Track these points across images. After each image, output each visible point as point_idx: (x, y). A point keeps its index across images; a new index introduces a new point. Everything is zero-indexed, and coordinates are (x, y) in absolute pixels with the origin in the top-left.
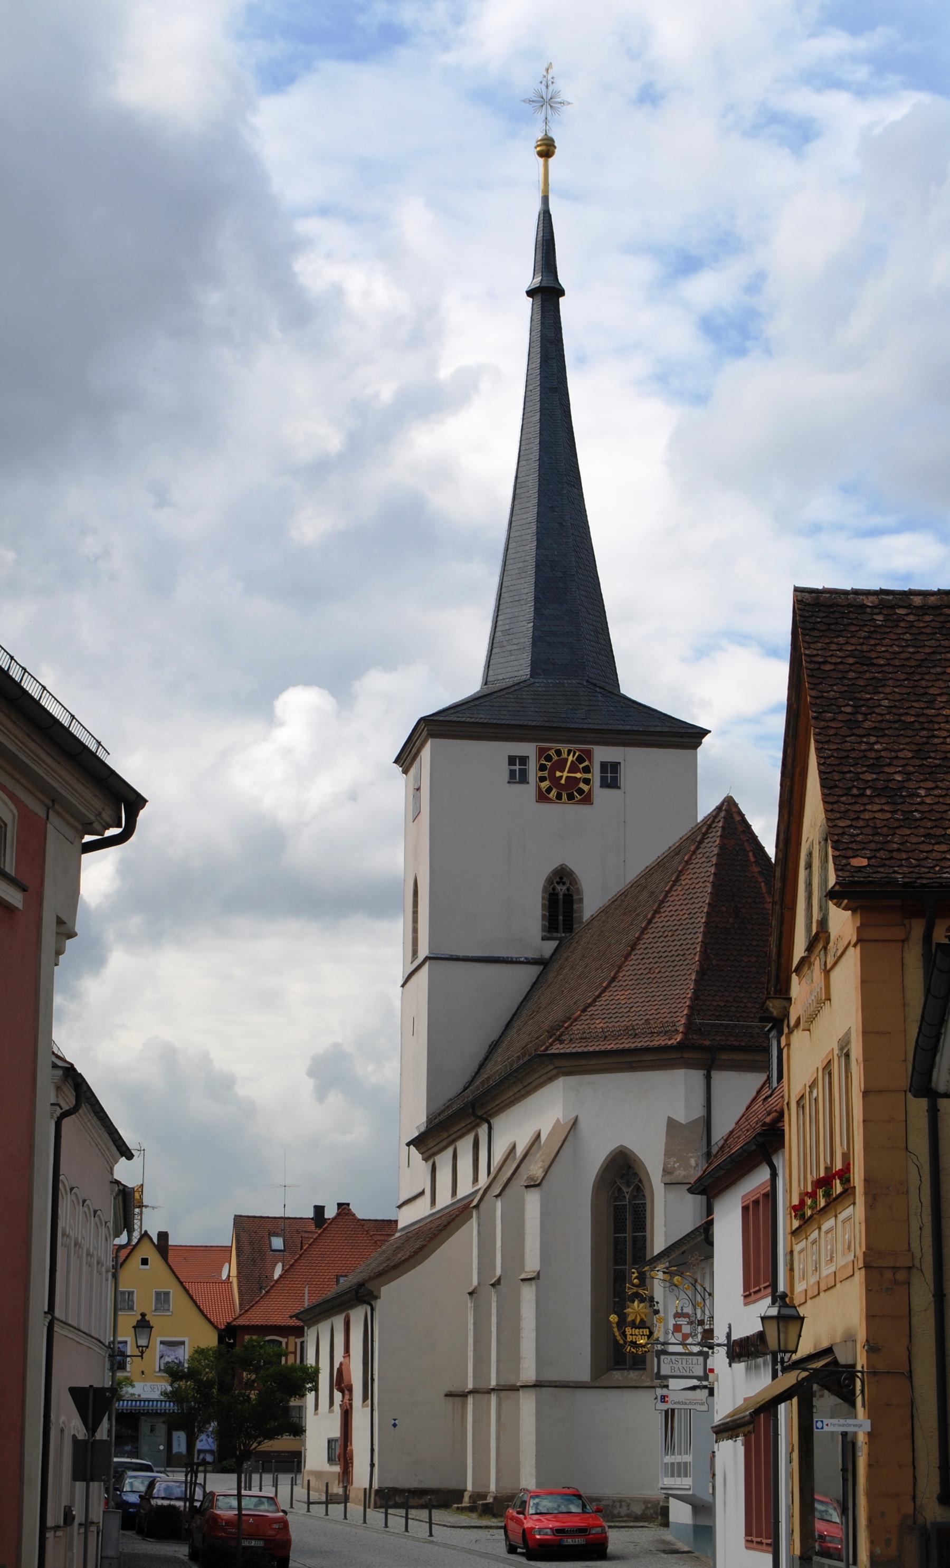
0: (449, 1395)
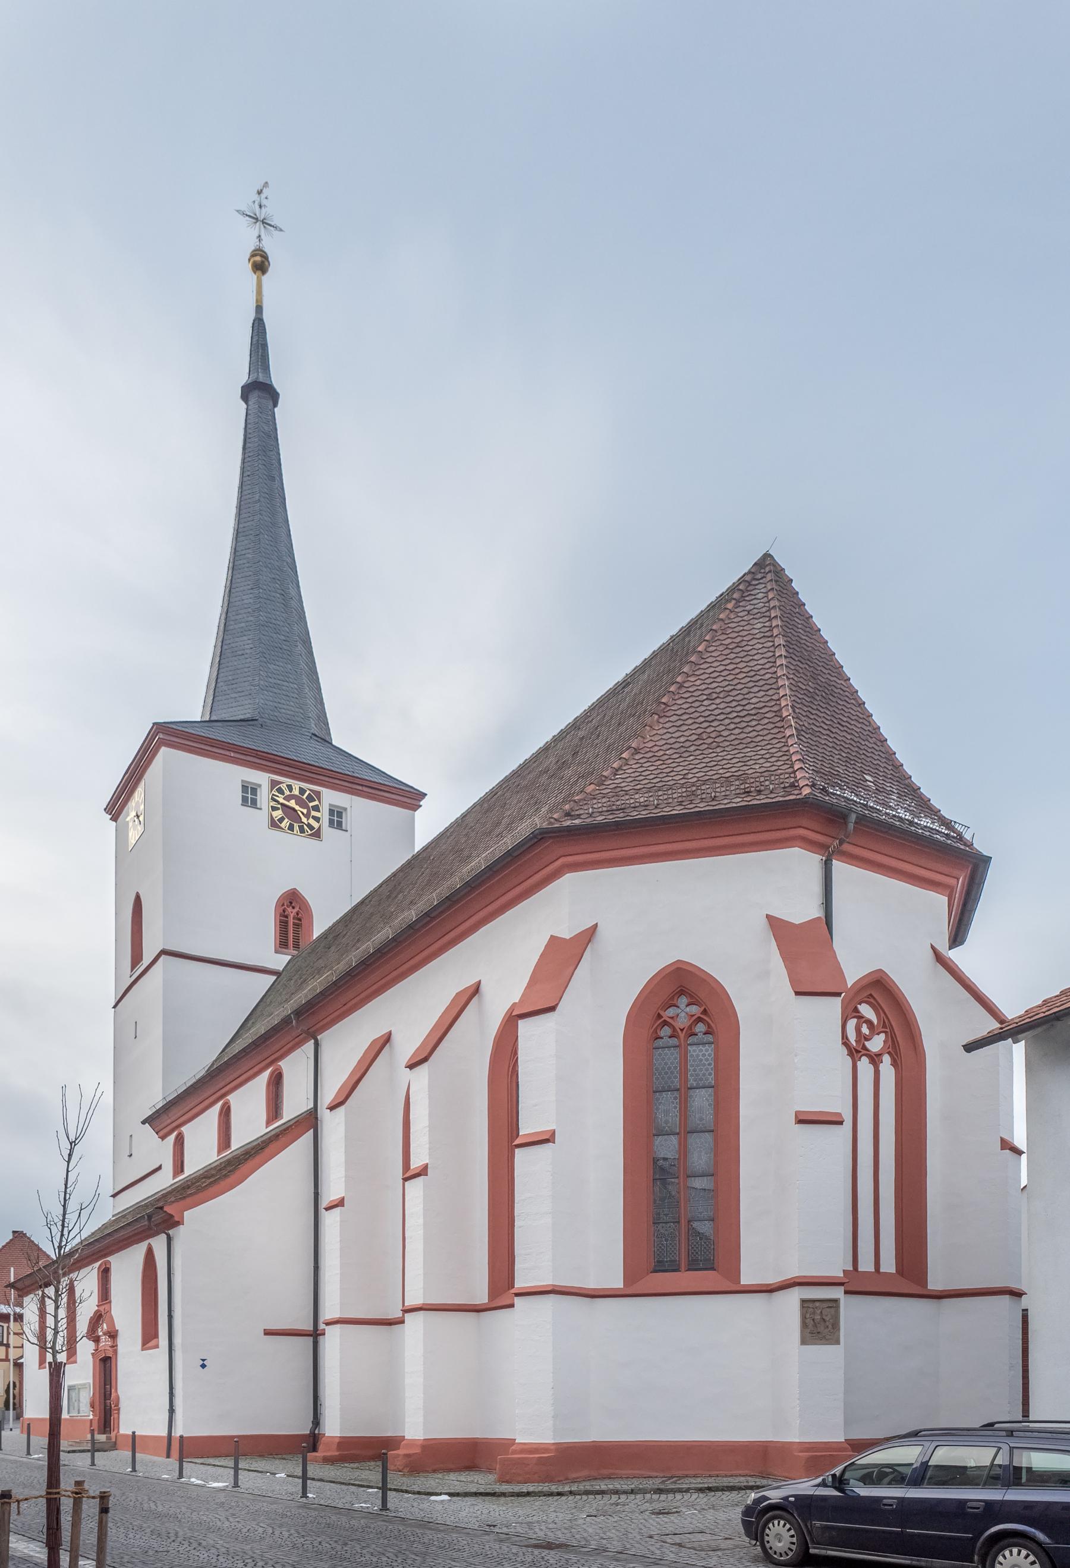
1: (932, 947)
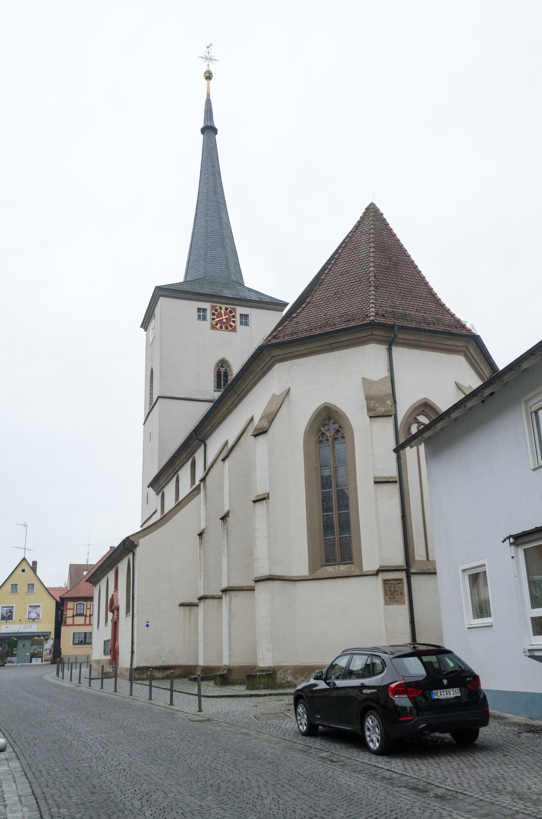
0: (182, 605)
1: (456, 383)
